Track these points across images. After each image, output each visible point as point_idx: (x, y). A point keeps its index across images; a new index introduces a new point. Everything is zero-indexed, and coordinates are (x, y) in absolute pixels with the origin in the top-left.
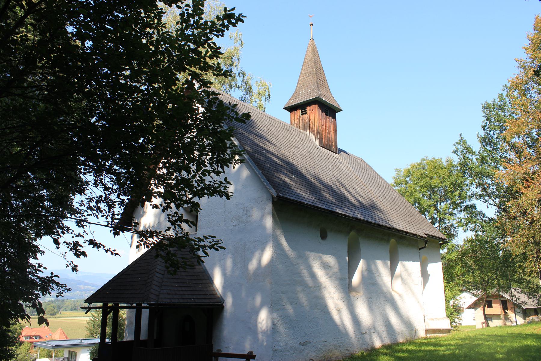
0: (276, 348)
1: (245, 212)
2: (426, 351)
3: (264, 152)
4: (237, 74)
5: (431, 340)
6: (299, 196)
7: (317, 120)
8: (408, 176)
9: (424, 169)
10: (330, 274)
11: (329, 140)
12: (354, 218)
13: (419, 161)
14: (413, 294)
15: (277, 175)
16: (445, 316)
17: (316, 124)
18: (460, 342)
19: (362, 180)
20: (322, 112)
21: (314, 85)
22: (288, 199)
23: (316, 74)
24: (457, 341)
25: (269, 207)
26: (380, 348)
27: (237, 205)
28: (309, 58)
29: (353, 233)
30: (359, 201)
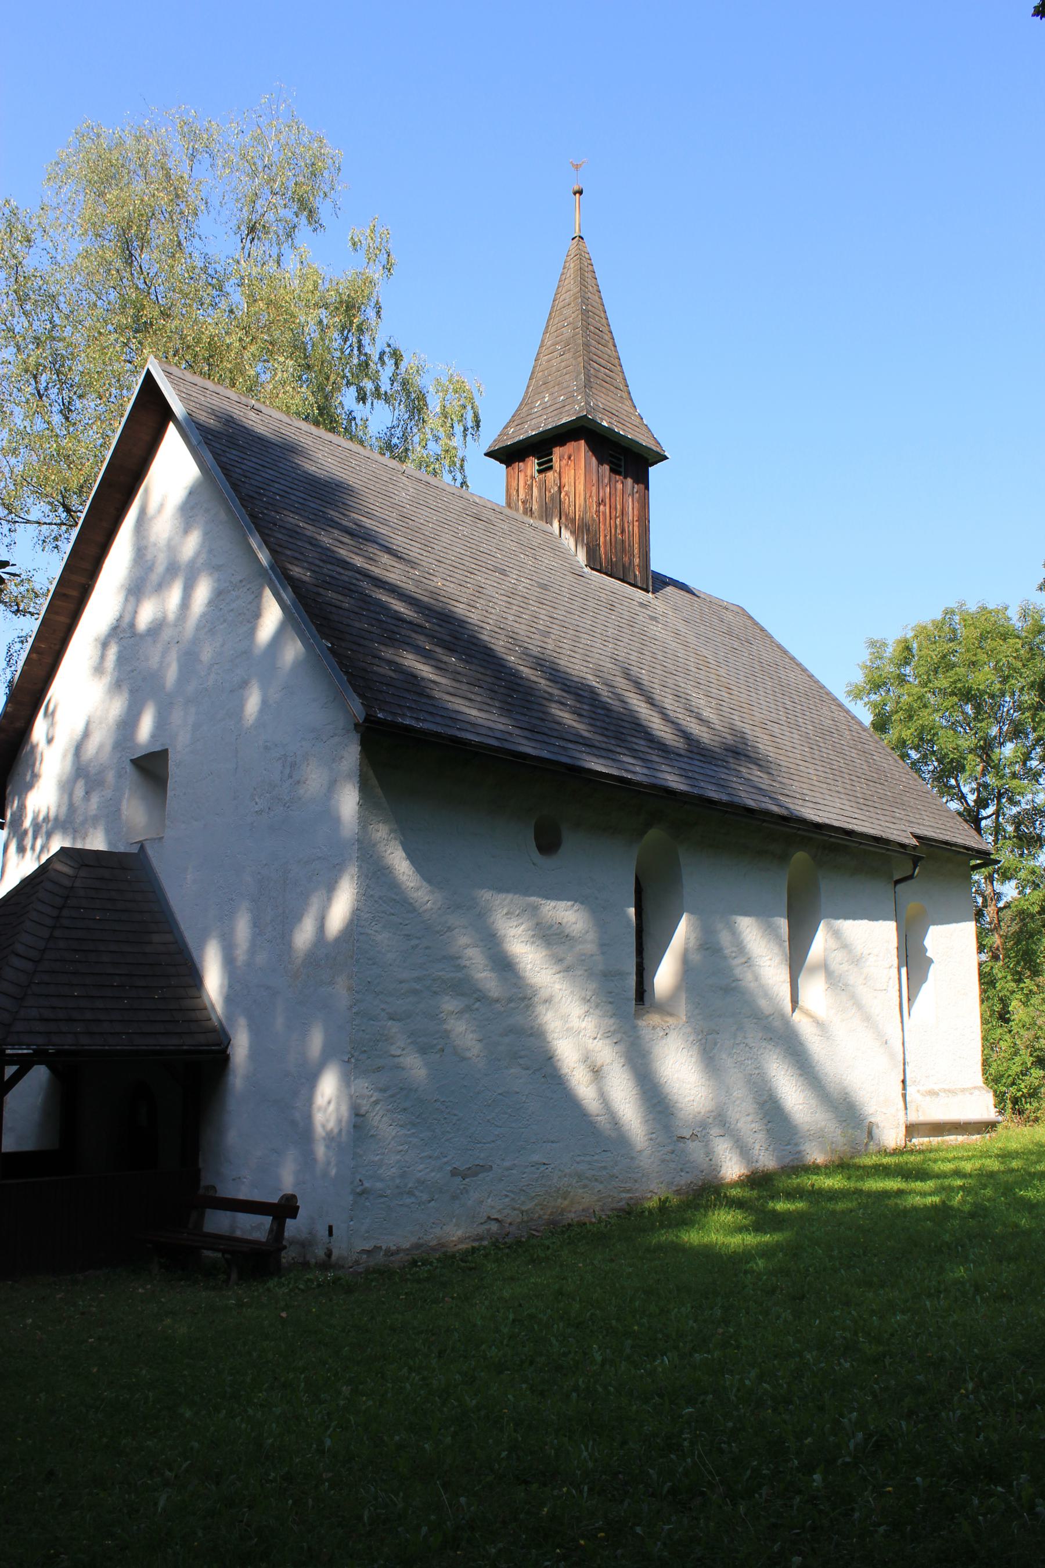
0: (367, 1185)
1: (287, 771)
2: (869, 1194)
3: (358, 586)
4: (375, 357)
5: (912, 1158)
6: (453, 718)
7: (581, 487)
8: (906, 662)
9: (951, 640)
10: (569, 959)
11: (621, 547)
12: (654, 786)
13: (939, 616)
14: (867, 1018)
15: (388, 653)
16: (979, 1079)
17: (580, 501)
18: (994, 1165)
19: (722, 672)
20: (601, 462)
21: (576, 378)
22: (408, 729)
23: (586, 345)
24: (988, 1162)
25: (351, 754)
26: (734, 1185)
27: (266, 748)
28: (567, 297)
29: (654, 834)
30: (686, 736)
